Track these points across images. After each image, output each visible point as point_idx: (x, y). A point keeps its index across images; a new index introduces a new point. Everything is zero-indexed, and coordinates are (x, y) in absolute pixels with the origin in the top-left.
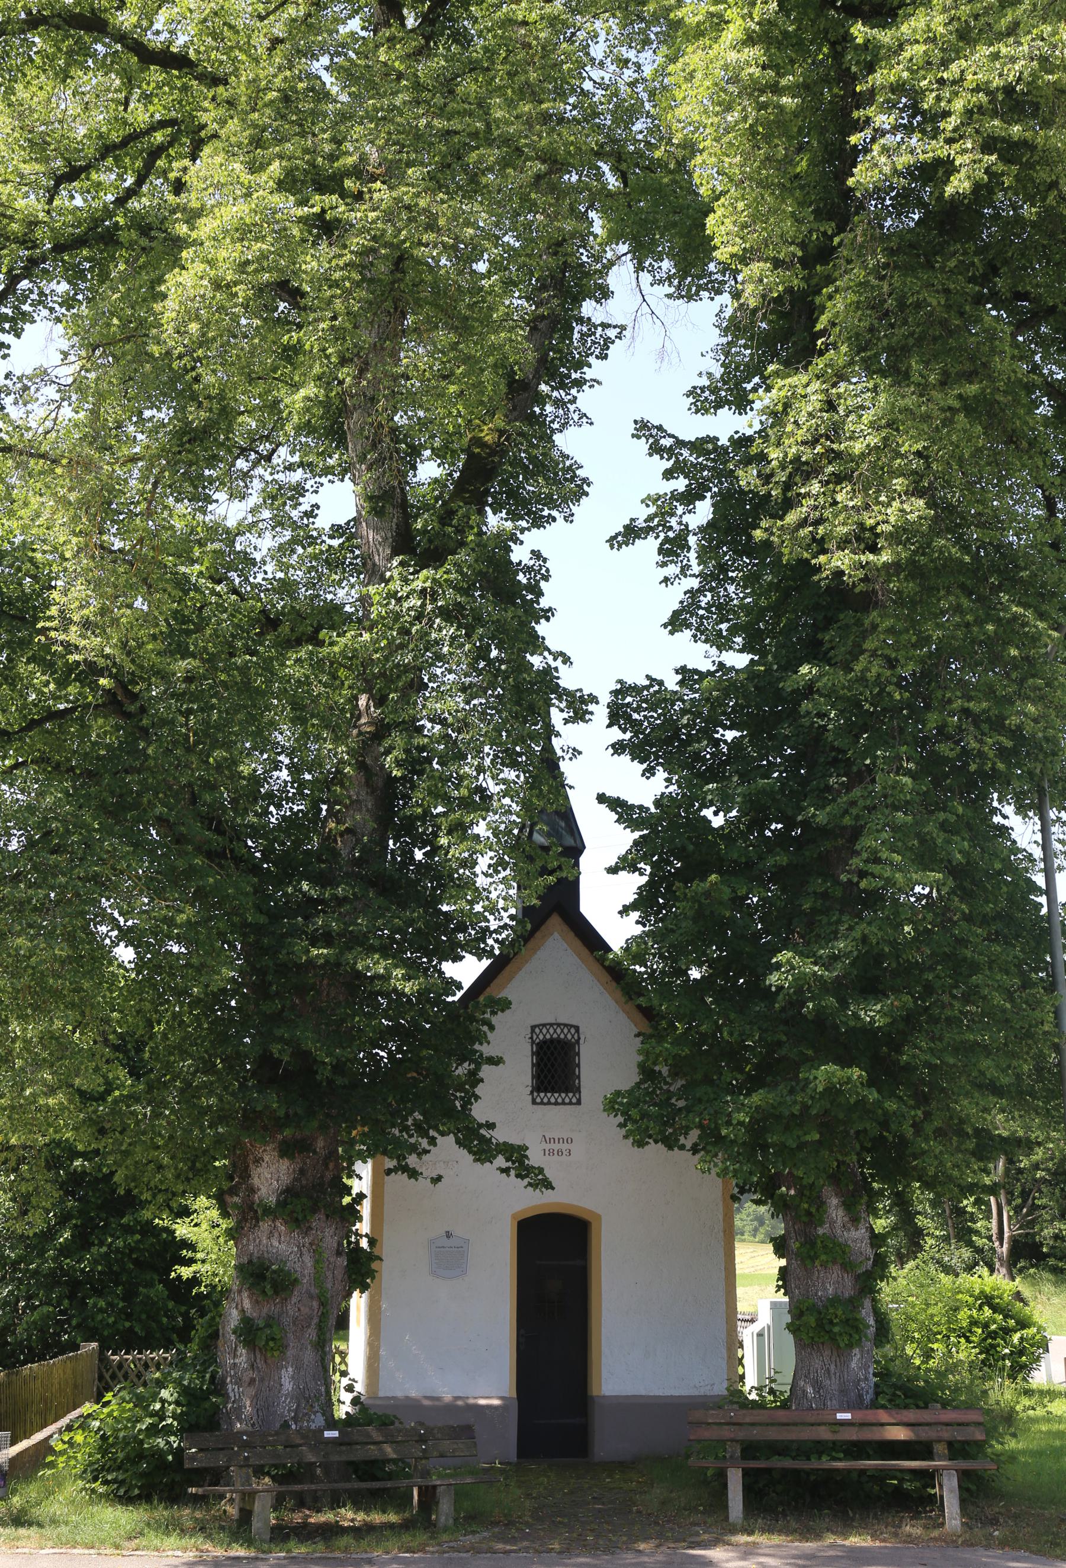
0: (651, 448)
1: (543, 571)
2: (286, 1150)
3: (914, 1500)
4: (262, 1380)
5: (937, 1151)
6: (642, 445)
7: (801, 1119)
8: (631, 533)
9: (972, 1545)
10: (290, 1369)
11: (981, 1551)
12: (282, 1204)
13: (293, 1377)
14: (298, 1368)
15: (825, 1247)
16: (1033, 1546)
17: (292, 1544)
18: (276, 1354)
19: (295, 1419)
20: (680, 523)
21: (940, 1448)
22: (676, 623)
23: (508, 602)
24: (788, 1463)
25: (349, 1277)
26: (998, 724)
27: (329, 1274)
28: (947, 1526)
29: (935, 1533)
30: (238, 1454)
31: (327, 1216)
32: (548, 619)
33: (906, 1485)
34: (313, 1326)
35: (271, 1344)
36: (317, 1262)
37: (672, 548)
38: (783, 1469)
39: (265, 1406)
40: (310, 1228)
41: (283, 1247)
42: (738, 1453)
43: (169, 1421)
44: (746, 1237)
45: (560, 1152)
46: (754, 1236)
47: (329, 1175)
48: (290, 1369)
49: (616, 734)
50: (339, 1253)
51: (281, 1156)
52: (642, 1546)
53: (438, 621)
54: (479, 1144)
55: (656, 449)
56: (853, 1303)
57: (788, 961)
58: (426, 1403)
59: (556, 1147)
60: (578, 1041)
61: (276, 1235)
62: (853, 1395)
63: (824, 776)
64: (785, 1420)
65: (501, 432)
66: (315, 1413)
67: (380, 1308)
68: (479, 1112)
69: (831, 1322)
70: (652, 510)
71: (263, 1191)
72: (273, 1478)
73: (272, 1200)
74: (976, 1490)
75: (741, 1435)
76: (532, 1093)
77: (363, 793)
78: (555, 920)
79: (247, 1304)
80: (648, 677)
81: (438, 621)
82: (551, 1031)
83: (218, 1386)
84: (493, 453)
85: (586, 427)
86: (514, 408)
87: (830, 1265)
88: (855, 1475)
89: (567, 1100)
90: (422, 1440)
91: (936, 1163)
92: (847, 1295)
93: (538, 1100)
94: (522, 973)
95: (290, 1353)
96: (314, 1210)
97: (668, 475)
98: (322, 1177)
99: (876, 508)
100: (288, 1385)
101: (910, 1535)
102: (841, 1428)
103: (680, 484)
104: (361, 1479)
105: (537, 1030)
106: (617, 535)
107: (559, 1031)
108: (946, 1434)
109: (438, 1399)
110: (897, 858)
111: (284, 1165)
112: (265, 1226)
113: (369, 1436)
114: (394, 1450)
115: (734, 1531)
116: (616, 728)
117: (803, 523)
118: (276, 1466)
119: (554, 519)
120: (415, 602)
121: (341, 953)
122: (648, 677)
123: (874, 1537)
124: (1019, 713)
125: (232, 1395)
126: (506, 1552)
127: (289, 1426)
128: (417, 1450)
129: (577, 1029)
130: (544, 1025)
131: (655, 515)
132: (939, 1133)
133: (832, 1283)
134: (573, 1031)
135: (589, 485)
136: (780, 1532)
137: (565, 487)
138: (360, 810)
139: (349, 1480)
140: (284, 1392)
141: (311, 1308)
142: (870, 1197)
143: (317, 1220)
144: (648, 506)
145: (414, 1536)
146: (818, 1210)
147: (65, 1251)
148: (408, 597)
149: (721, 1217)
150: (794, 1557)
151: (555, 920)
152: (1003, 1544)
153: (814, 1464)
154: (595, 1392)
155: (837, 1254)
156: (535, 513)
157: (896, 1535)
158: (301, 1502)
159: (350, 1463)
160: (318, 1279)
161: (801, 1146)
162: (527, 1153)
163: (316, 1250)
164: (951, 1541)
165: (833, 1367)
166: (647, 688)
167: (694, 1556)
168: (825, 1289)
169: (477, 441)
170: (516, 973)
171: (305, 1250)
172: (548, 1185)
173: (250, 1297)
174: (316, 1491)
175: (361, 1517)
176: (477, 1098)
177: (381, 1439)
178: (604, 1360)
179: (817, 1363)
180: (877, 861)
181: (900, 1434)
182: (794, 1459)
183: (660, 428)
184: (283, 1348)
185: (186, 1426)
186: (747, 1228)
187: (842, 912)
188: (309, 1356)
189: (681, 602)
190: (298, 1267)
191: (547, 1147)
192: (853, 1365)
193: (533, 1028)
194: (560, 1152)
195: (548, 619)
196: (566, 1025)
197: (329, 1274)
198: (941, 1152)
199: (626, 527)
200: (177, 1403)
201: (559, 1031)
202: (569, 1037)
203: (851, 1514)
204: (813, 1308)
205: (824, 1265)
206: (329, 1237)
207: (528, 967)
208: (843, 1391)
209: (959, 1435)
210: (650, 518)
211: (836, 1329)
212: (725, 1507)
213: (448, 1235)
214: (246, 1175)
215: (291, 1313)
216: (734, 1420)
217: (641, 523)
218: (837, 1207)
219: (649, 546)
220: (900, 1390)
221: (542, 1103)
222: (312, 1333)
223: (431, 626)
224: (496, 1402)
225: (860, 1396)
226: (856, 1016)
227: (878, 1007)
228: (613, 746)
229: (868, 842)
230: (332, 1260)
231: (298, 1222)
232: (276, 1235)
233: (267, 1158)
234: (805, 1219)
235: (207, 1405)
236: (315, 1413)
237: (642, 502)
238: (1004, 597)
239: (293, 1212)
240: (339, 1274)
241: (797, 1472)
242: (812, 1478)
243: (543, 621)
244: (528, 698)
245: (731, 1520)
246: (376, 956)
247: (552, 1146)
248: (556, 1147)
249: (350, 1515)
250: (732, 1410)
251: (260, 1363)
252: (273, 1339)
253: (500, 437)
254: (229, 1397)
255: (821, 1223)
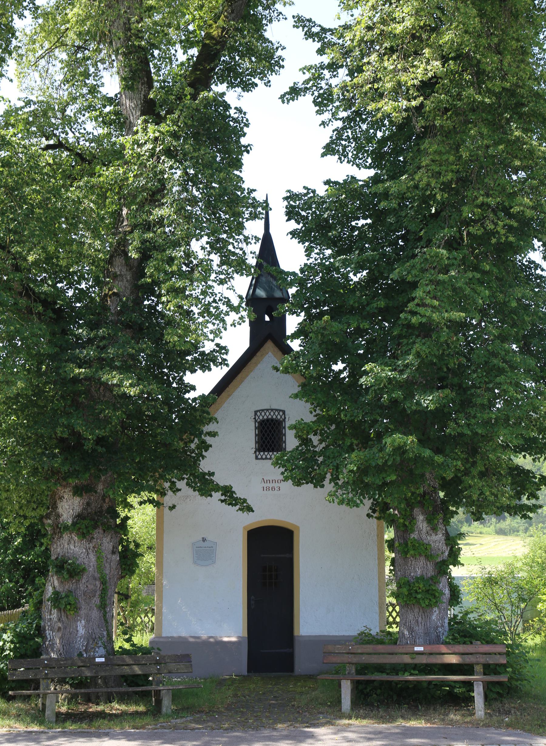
0: (306, 34)
1: (244, 121)
2: (78, 491)
3: (460, 699)
4: (65, 628)
5: (480, 485)
6: (300, 33)
7: (381, 469)
8: (294, 92)
9: (489, 726)
10: (83, 622)
11: (493, 730)
12: (74, 524)
13: (85, 626)
14: (88, 621)
15: (413, 546)
16: (528, 727)
17: (68, 724)
18: (72, 613)
19: (86, 651)
20: (327, 84)
21: (478, 668)
22: (329, 150)
23: (217, 140)
24: (384, 677)
25: (121, 567)
26: (507, 211)
27: (107, 565)
28: (476, 715)
29: (468, 719)
30: (42, 672)
31: (104, 531)
32: (248, 152)
33: (456, 690)
34: (97, 596)
35: (68, 607)
36: (98, 558)
37: (323, 101)
38: (381, 681)
39: (67, 643)
40: (93, 538)
41: (77, 549)
42: (353, 671)
43: (7, 652)
44: (520, 533)
45: (273, 489)
46: (526, 533)
47: (105, 506)
48: (83, 622)
49: (293, 225)
50: (113, 553)
51: (74, 495)
52: (279, 726)
53: (163, 158)
54: (205, 485)
55: (309, 35)
56: (434, 580)
57: (371, 370)
58: (191, 640)
59: (271, 485)
60: (284, 420)
61: (72, 542)
62: (433, 636)
63: (413, 248)
64: (383, 651)
65: (223, 29)
66: (99, 647)
67: (162, 584)
68: (205, 466)
69: (416, 592)
70: (308, 75)
71: (65, 516)
72: (71, 685)
73: (70, 522)
74: (497, 694)
75: (355, 660)
76: (255, 452)
77: (124, 270)
78: (269, 345)
79: (56, 583)
80: (305, 188)
81: (163, 158)
82: (268, 414)
83: (40, 631)
84: (218, 43)
85: (282, 21)
86: (233, 12)
87: (418, 557)
88: (425, 685)
89: (264, 457)
90: (158, 663)
91: (478, 492)
92: (429, 575)
93: (259, 457)
94: (249, 378)
95: (83, 612)
96: (95, 527)
97: (321, 52)
98: (101, 507)
99: (411, 70)
100: (81, 631)
101: (452, 720)
102: (417, 656)
103: (326, 59)
104: (129, 685)
105: (258, 414)
106: (285, 94)
107: (272, 413)
108: (482, 659)
109: (198, 638)
110: (436, 303)
111: (77, 500)
112: (66, 536)
113: (123, 660)
114: (140, 669)
115: (342, 716)
116: (293, 221)
117: (367, 82)
118: (72, 678)
119: (256, 85)
120: (149, 146)
121: (97, 371)
122: (305, 188)
123: (427, 721)
124: (521, 205)
125: (48, 637)
126: (193, 729)
127: (82, 655)
128: (153, 669)
129: (284, 412)
130: (263, 410)
131: (310, 80)
132: (482, 475)
133: (420, 568)
134: (281, 413)
135: (283, 60)
136: (371, 718)
137: (268, 61)
138: (122, 281)
139: (121, 686)
140: (79, 635)
141: (95, 585)
142: (445, 515)
143: (97, 533)
144: (304, 73)
145: (143, 719)
146: (410, 523)
147: (18, 550)
148: (145, 143)
149: (376, 527)
150: (370, 733)
151: (269, 345)
152: (508, 726)
153: (395, 678)
154: (296, 633)
155: (423, 550)
156: (245, 82)
157: (443, 720)
158: (88, 699)
159: (123, 676)
160: (100, 568)
161: (385, 484)
162: (233, 490)
163: (98, 551)
164: (477, 725)
165: (420, 619)
166: (305, 195)
167: (305, 732)
168: (416, 572)
169: (209, 36)
170: (245, 378)
171: (90, 551)
172: (250, 509)
173: (58, 579)
174: (98, 693)
175: (123, 707)
176: (203, 457)
177: (131, 662)
178: (301, 614)
179: (411, 617)
180: (424, 305)
181: (453, 659)
182: (388, 674)
183: (310, 20)
184: (76, 608)
185: (18, 655)
186: (521, 528)
187: (417, 336)
188: (95, 614)
189: (331, 137)
190: (86, 561)
191: (265, 485)
192: (434, 617)
193: (256, 412)
194: (273, 489)
195: (248, 152)
196: (276, 410)
197: (107, 565)
198: (483, 486)
199: (291, 88)
200: (12, 642)
201: (272, 413)
202: (279, 417)
203: (420, 707)
204: (408, 583)
205: (414, 556)
206: (107, 543)
207: (252, 374)
208: (427, 634)
209: (491, 660)
210: (307, 82)
211: (419, 596)
212: (339, 702)
213: (204, 540)
214: (54, 506)
215: (82, 588)
216: (352, 651)
217: (300, 86)
218: (423, 521)
219: (306, 101)
220: (464, 632)
221: (262, 459)
222: (96, 600)
223: (159, 162)
224: (234, 639)
225: (438, 636)
226: (418, 403)
227: (431, 398)
228: (291, 233)
229: (419, 293)
230: (109, 556)
231: (84, 535)
232: (72, 542)
233: (66, 496)
234: (402, 529)
235: (31, 643)
236: (99, 647)
237: (300, 70)
238: (514, 125)
239: (79, 529)
240: (114, 565)
241: (390, 682)
242: (399, 686)
243: (245, 153)
244: (230, 204)
245: (343, 710)
246: (114, 373)
247: (268, 485)
248: (271, 485)
249: (117, 706)
250: (350, 645)
251: (64, 618)
252: (70, 604)
253: (222, 32)
254: (47, 638)
255: (413, 531)
